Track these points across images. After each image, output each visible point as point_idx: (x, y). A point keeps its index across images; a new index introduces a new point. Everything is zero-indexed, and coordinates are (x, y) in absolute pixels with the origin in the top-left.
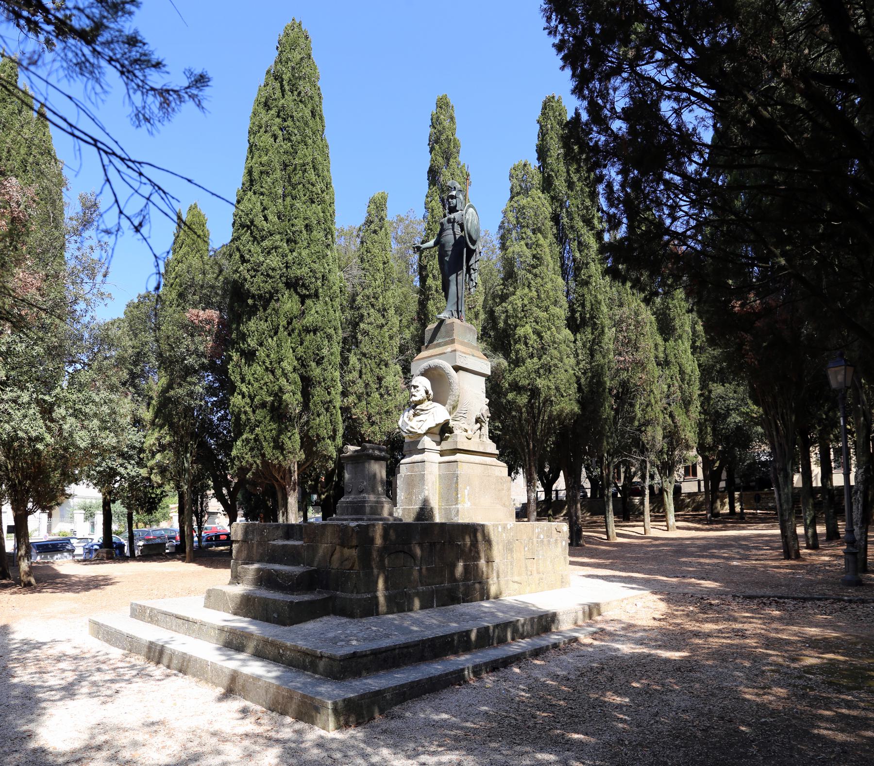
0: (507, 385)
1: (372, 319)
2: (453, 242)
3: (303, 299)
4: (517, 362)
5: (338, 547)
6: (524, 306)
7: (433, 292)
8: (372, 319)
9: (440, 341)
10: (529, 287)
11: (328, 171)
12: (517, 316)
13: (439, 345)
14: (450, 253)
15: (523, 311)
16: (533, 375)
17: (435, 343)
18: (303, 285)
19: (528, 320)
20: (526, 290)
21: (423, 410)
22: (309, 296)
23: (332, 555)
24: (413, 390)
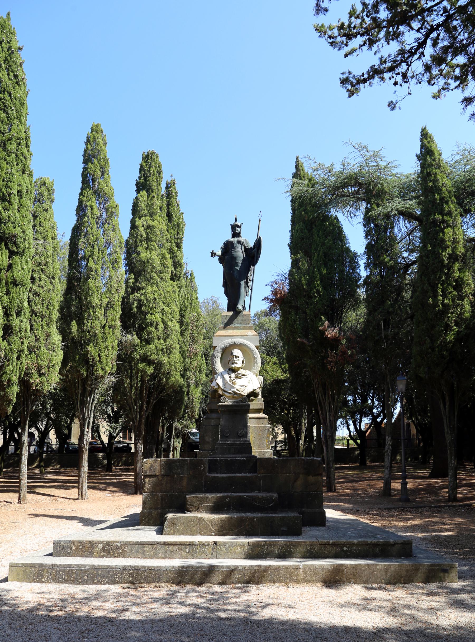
0: (138, 357)
1: (42, 283)
2: (243, 258)
3: (12, 254)
4: (148, 342)
5: (301, 476)
6: (155, 299)
7: (93, 273)
8: (42, 283)
9: (237, 325)
10: (157, 286)
11: (27, 146)
12: (149, 306)
13: (237, 328)
14: (240, 265)
15: (154, 303)
16: (160, 353)
17: (232, 326)
18: (15, 243)
19: (157, 311)
20: (155, 288)
21: (243, 375)
22: (17, 253)
23: (295, 481)
24: (235, 359)
